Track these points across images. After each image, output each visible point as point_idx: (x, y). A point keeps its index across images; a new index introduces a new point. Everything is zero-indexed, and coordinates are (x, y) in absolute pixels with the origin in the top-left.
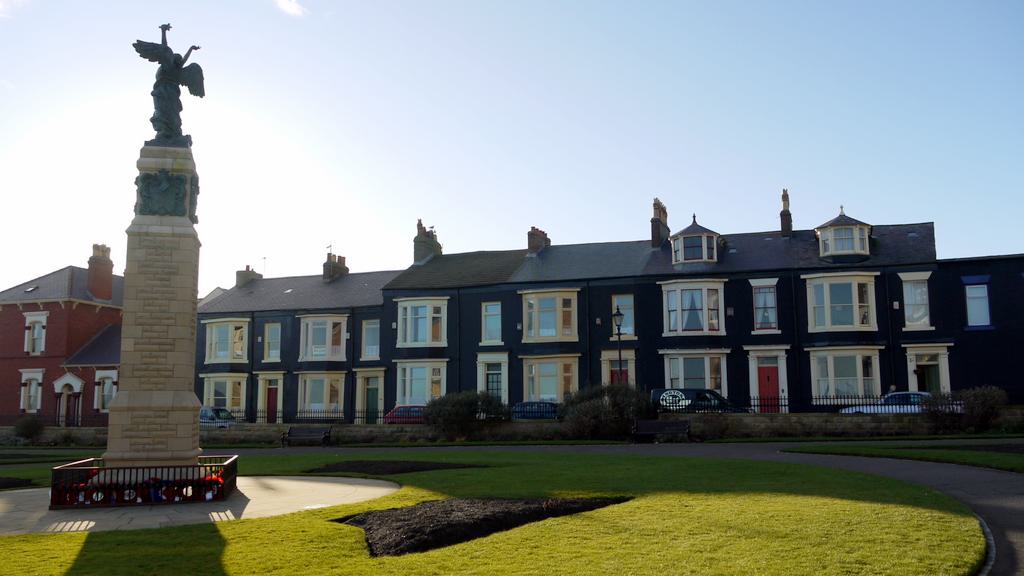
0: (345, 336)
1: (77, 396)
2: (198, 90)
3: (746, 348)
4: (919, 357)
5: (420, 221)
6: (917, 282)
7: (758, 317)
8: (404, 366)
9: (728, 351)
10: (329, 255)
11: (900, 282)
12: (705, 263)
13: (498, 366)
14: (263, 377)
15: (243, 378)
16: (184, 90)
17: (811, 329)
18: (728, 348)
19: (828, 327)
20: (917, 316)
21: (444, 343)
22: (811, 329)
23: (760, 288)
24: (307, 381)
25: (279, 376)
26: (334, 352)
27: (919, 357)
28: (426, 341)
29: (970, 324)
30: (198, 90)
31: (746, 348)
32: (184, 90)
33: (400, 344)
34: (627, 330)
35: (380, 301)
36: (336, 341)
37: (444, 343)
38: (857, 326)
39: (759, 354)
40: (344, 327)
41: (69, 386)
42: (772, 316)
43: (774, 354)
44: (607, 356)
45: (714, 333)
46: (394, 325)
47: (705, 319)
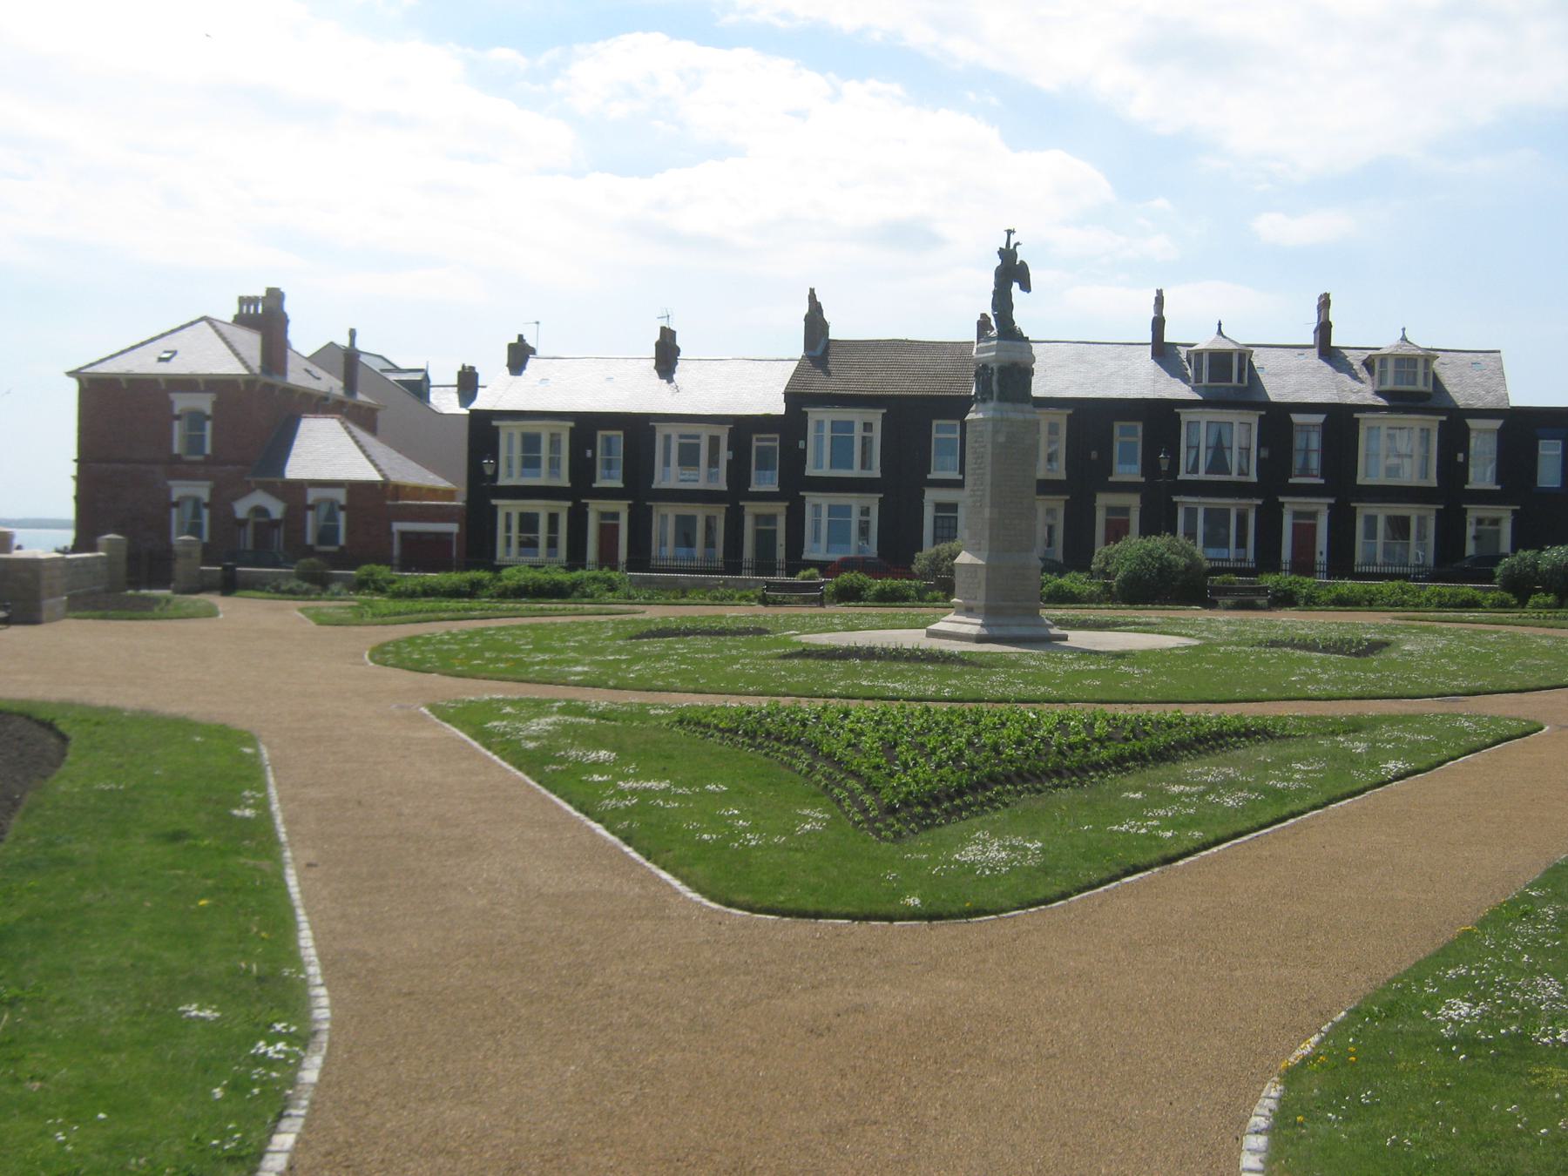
0: (725, 455)
1: (275, 524)
2: (1026, 287)
3: (1281, 499)
4: (1480, 521)
5: (812, 291)
6: (1486, 431)
7: (1298, 461)
8: (817, 501)
9: (1259, 502)
10: (663, 329)
11: (1467, 430)
12: (1235, 388)
13: (771, 519)
14: (595, 509)
15: (562, 507)
16: (1016, 286)
17: (1361, 480)
18: (1258, 497)
19: (826, 471)
20: (1482, 476)
21: (876, 472)
22: (1361, 480)
23: (1302, 426)
24: (817, 505)
25: (622, 508)
26: (711, 477)
27: (1480, 521)
28: (1409, 476)
29: (1540, 485)
30: (1026, 287)
31: (1281, 499)
32: (1016, 286)
33: (810, 471)
34: (1127, 470)
35: (779, 408)
36: (713, 462)
37: (876, 472)
38: (856, 472)
39: (1297, 508)
40: (724, 444)
41: (260, 511)
42: (1315, 462)
43: (1314, 508)
44: (1103, 500)
45: (1243, 479)
46: (801, 444)
47: (1234, 460)
